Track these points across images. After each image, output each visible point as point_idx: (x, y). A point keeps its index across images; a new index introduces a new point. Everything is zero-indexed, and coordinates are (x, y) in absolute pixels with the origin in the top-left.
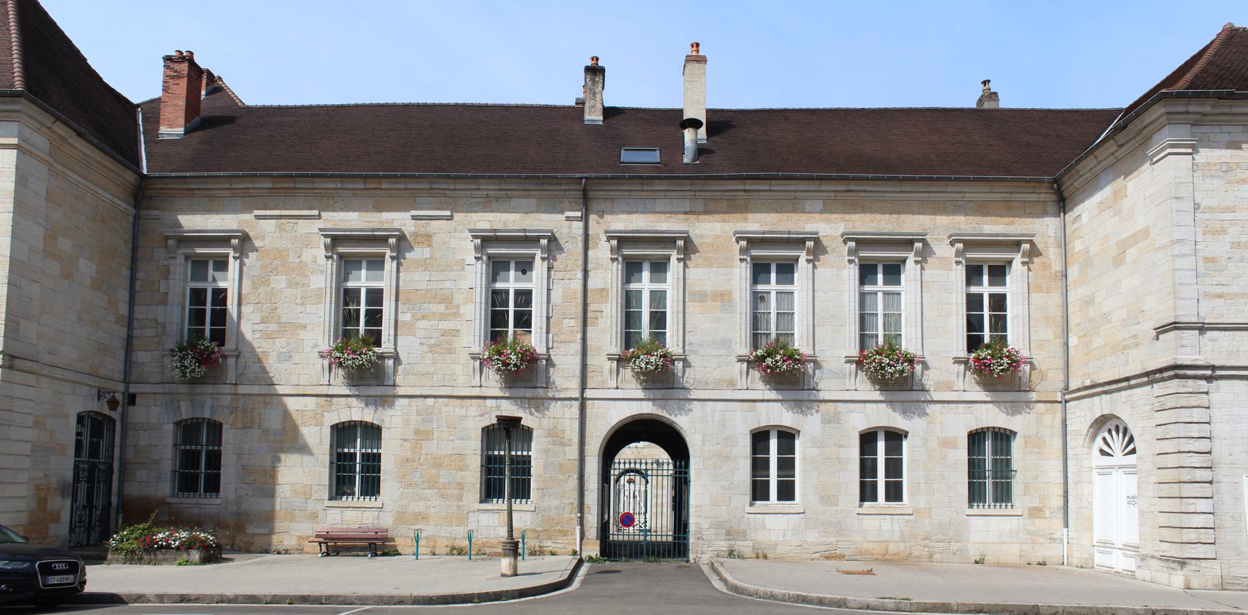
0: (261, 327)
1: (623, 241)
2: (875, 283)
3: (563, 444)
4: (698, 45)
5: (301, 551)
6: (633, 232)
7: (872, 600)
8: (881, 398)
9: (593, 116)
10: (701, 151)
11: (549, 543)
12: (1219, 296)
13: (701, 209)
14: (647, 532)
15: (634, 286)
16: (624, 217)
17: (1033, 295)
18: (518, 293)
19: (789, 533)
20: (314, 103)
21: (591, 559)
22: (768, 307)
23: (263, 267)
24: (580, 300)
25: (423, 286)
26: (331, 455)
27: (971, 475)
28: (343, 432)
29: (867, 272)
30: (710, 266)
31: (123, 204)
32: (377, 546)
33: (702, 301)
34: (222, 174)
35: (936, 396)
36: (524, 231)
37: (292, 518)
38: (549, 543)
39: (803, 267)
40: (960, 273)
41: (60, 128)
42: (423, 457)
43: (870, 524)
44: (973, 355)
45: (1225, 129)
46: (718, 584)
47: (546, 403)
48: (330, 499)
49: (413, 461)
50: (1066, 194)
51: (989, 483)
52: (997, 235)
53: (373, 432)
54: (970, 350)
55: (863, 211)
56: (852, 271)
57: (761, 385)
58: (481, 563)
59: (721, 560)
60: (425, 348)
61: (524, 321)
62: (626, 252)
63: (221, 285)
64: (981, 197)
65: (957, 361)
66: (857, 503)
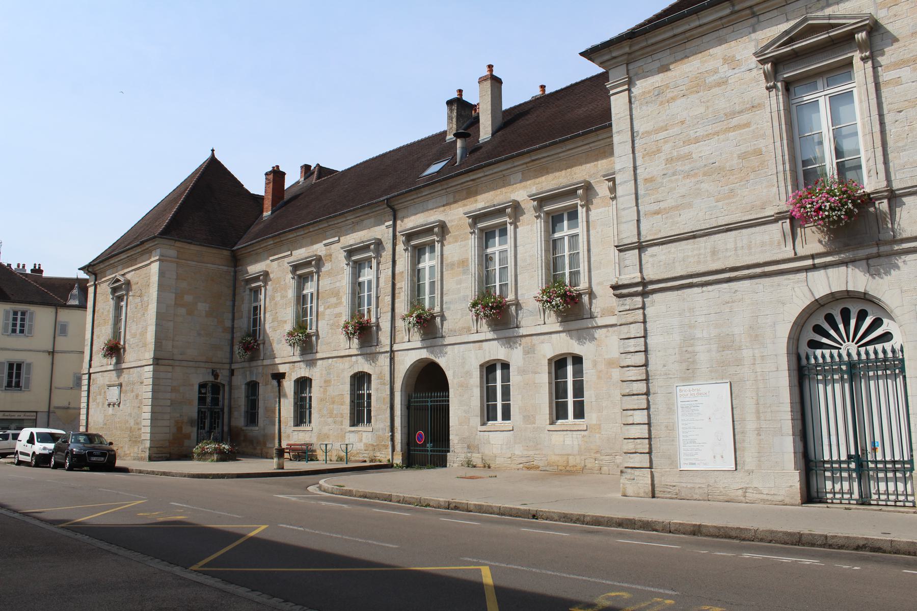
8: (561, 329)
12: (657, 213)
16: (413, 218)
30: (456, 241)
31: (225, 268)
41: (178, 244)
43: (557, 438)
45: (655, 57)
55: (548, 173)
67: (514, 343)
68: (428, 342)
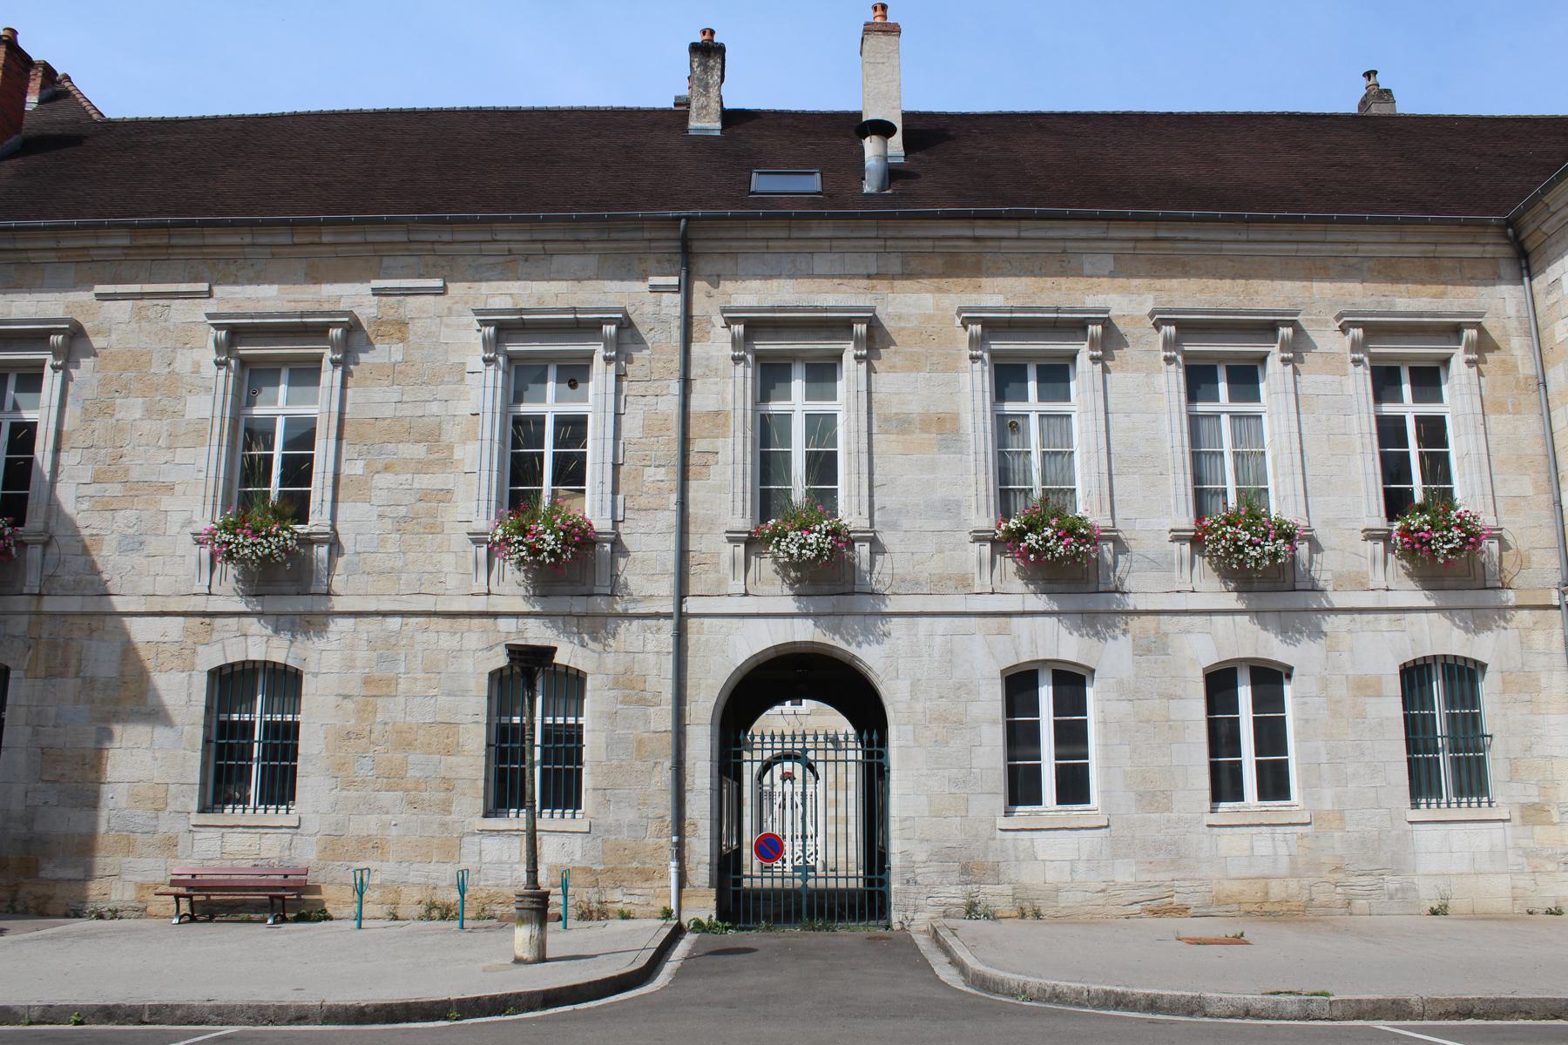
0: (91, 490)
1: (755, 326)
2: (1215, 398)
3: (643, 702)
4: (884, 7)
5: (141, 912)
6: (773, 309)
7: (1255, 999)
8: (1240, 606)
9: (705, 122)
10: (893, 174)
11: (617, 895)
13: (897, 269)
14: (806, 869)
15: (775, 407)
16: (756, 284)
17: (1492, 419)
18: (561, 421)
19: (1081, 867)
20: (222, 112)
21: (699, 926)
22: (1026, 443)
23: (103, 384)
24: (674, 433)
25: (387, 411)
26: (207, 726)
27: (1412, 746)
28: (231, 683)
29: (1199, 379)
30: (916, 368)
32: (287, 902)
33: (903, 431)
34: (42, 223)
35: (1339, 600)
36: (574, 310)
37: (129, 848)
38: (617, 895)
39: (1085, 371)
40: (1360, 382)
42: (378, 729)
43: (1233, 843)
44: (1397, 525)
46: (947, 974)
47: (611, 623)
48: (203, 810)
49: (358, 736)
50: (1529, 245)
51: (1444, 760)
52: (1420, 314)
53: (285, 682)
54: (1391, 515)
55: (1186, 274)
56: (1173, 376)
57: (1018, 585)
58: (482, 935)
59: (952, 923)
60: (388, 524)
61: (571, 472)
62: (761, 345)
63: (28, 415)
64: (1386, 251)
65: (1370, 535)
66: (1207, 805)
67: (1108, 627)
68: (825, 604)
